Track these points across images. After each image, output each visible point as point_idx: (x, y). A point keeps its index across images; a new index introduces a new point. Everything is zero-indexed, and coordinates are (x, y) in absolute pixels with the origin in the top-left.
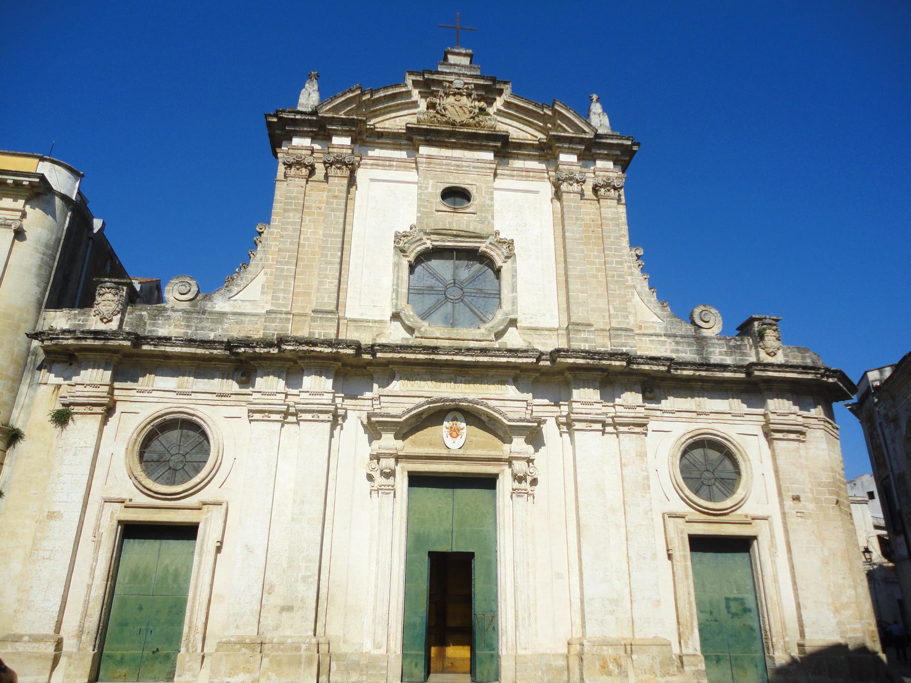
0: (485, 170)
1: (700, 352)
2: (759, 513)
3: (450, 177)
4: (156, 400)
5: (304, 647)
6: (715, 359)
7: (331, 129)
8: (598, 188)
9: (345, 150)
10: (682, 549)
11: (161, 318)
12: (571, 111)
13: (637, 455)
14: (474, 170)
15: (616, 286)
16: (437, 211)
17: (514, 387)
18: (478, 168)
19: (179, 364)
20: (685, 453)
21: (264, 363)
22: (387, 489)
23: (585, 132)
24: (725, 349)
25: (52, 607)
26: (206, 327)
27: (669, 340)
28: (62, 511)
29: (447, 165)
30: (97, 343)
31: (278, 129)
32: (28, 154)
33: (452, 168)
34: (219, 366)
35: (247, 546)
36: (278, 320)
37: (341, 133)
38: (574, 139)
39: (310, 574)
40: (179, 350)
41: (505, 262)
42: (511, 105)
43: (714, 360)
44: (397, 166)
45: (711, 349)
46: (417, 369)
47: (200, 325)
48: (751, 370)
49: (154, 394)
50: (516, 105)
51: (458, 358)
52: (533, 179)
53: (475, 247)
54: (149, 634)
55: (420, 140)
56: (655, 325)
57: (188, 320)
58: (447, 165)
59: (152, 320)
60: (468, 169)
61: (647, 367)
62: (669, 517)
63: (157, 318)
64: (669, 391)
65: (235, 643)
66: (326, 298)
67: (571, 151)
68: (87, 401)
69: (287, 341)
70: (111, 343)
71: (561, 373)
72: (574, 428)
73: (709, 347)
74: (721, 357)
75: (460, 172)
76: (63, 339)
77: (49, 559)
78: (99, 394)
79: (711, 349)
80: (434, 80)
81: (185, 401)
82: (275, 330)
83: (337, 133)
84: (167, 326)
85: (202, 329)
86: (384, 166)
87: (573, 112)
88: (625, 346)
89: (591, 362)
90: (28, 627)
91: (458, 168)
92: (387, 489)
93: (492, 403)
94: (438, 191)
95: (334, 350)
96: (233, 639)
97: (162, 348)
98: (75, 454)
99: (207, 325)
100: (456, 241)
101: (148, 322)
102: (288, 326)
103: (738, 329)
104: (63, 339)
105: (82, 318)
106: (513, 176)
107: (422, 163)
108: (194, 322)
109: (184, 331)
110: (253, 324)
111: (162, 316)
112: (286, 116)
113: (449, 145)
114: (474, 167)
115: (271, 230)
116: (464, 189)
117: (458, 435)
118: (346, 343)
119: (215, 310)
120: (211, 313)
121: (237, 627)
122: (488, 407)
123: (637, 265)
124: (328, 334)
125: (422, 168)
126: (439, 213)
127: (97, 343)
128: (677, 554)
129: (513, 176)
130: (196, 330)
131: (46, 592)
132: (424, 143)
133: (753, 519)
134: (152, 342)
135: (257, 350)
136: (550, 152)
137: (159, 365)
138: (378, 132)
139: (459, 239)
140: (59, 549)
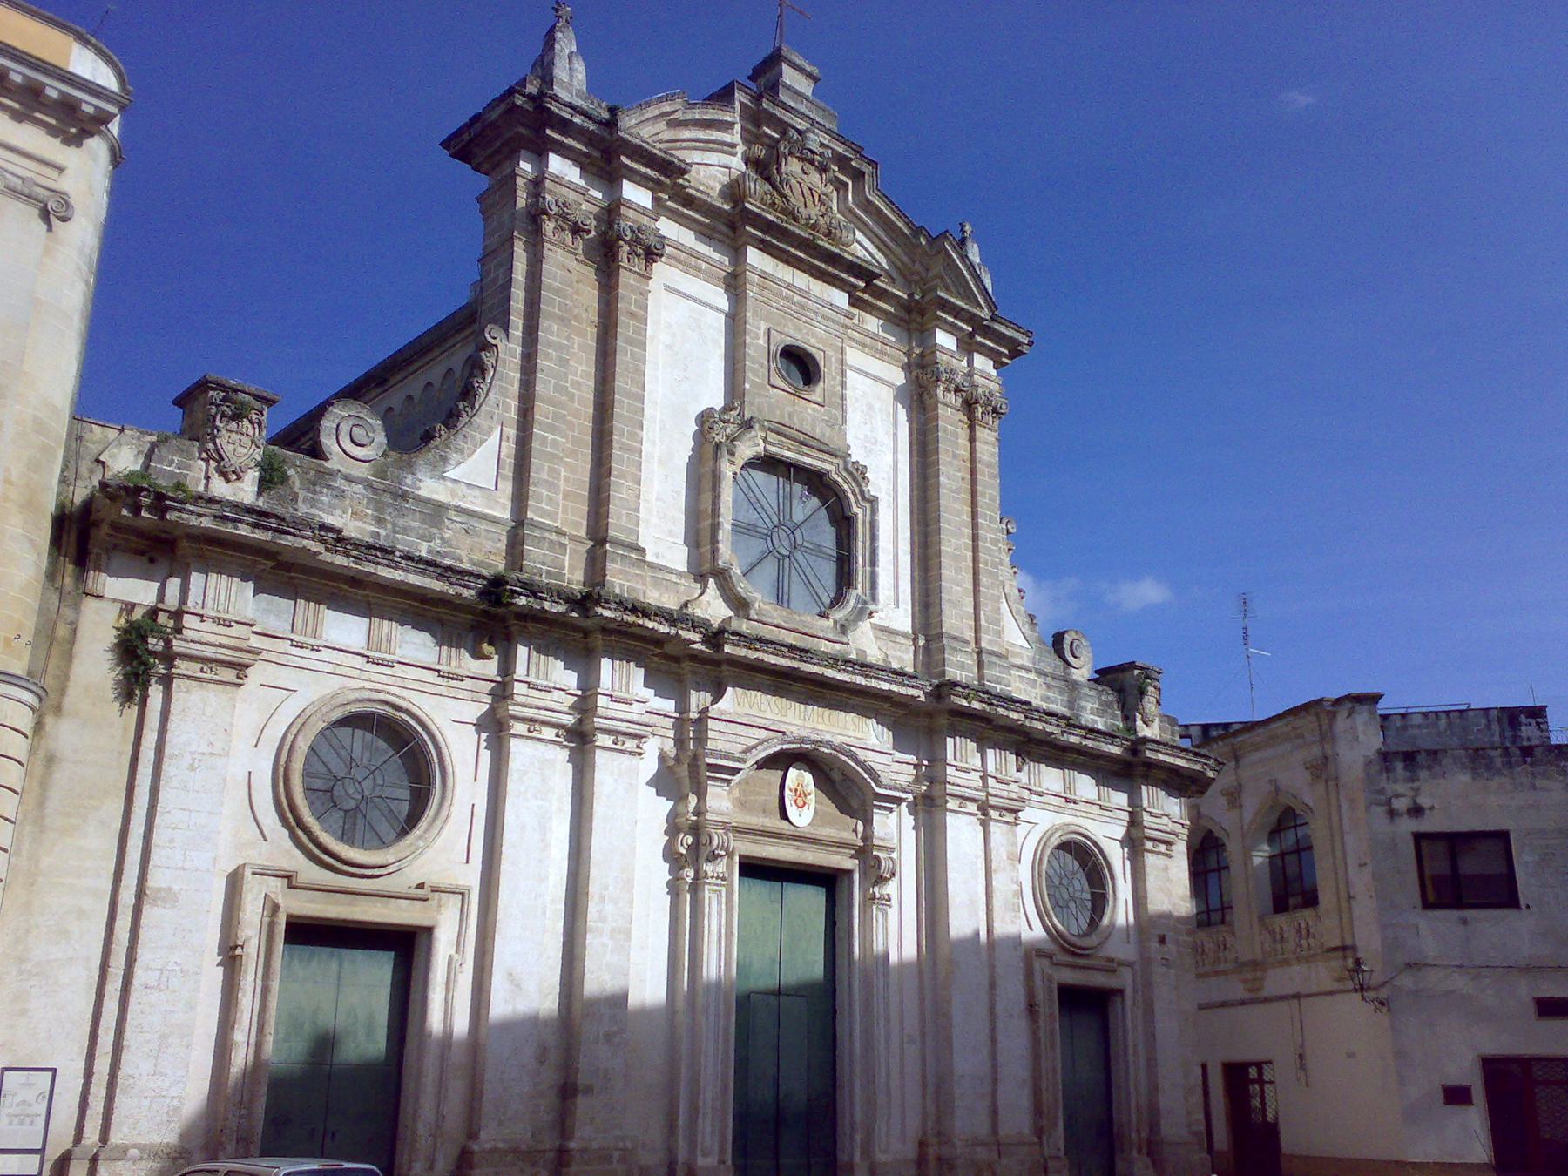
0: (836, 327)
1: (1071, 704)
2: (445, 881)
3: (790, 325)
4: (329, 668)
5: (616, 1155)
8: (545, 217)
10: (1049, 1007)
13: (1008, 858)
18: (829, 319)
21: (532, 627)
22: (717, 885)
25: (170, 1087)
26: (413, 529)
27: (1040, 680)
28: (176, 887)
30: (259, 535)
31: (523, 125)
33: (794, 308)
34: (445, 617)
35: (511, 974)
36: (546, 544)
37: (638, 178)
39: (615, 1028)
40: (402, 578)
44: (705, 272)
45: (1083, 703)
46: (759, 677)
47: (401, 522)
48: (1140, 747)
49: (325, 654)
52: (889, 360)
56: (1023, 652)
57: (379, 507)
59: (308, 490)
62: (254, 873)
63: (318, 489)
64: (547, 647)
66: (624, 518)
67: (952, 329)
68: (213, 656)
69: (607, 601)
70: (288, 541)
71: (716, 663)
72: (512, 732)
73: (1080, 699)
74: (1092, 717)
75: (804, 319)
76: (191, 512)
77: (158, 988)
79: (1083, 703)
80: (773, 115)
81: (384, 679)
82: (544, 564)
84: (339, 512)
85: (405, 530)
88: (1000, 683)
90: (125, 1130)
91: (801, 311)
92: (717, 885)
93: (862, 755)
95: (673, 631)
96: (501, 1145)
97: (370, 568)
98: (192, 768)
101: (302, 494)
102: (564, 560)
104: (191, 512)
105: (176, 459)
107: (753, 284)
109: (373, 528)
110: (492, 539)
111: (329, 487)
112: (557, 111)
113: (791, 260)
115: (510, 345)
116: (810, 355)
117: (805, 804)
118: (693, 622)
119: (420, 493)
121: (501, 1124)
122: (857, 761)
124: (634, 589)
126: (775, 390)
127: (259, 535)
128: (1043, 1010)
130: (395, 532)
131: (156, 1058)
133: (432, 891)
134: (354, 553)
135: (547, 605)
136: (919, 319)
137: (333, 594)
138: (688, 194)
139: (805, 449)
140: (177, 968)
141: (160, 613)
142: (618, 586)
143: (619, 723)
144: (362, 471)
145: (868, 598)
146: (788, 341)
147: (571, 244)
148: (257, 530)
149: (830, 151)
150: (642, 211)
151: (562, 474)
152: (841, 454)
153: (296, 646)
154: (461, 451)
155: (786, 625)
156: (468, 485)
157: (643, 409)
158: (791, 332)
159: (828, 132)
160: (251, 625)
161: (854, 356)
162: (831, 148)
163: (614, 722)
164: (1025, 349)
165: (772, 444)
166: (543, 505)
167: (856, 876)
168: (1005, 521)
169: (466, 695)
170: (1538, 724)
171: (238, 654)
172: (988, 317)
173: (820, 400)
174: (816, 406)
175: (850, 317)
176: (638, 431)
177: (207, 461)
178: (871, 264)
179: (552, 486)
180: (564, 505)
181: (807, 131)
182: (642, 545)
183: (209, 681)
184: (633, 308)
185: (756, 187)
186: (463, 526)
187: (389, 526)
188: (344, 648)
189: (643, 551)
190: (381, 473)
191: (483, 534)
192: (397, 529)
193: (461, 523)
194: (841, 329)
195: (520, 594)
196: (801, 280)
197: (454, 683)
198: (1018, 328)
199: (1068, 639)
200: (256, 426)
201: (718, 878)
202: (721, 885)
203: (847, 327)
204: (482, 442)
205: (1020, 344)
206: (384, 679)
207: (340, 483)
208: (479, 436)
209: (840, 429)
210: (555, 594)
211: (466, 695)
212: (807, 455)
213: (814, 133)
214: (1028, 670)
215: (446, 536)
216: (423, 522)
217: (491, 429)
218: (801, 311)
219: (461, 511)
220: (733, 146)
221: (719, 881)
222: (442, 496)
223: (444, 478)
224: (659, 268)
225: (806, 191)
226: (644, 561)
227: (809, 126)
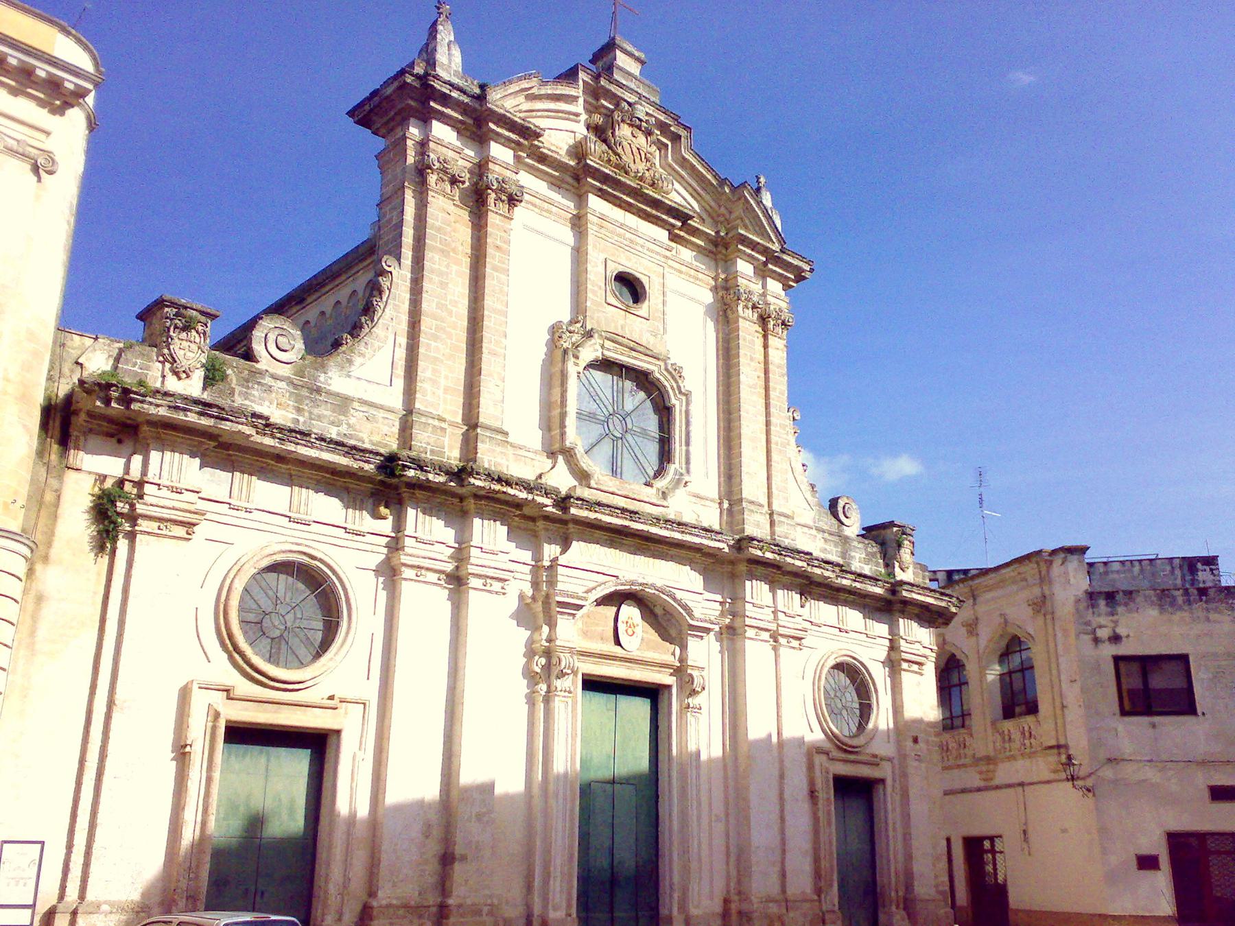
3: (622, 255)
4: (369, 547)
5: (486, 909)
6: (856, 566)
7: (493, 131)
10: (826, 793)
11: (256, 386)
14: (647, 252)
17: (702, 577)
18: (652, 251)
19: (293, 473)
20: (275, 568)
24: (863, 556)
27: (820, 535)
29: (619, 235)
30: (205, 422)
31: (412, 98)
32: (44, 14)
36: (430, 429)
37: (503, 141)
38: (758, 246)
39: (485, 810)
42: (686, 164)
43: (856, 568)
46: (598, 533)
47: (316, 411)
48: (898, 588)
50: (693, 166)
51: (654, 530)
53: (648, 369)
54: (258, 898)
55: (593, 186)
58: (619, 235)
59: (242, 386)
60: (641, 249)
61: (818, 571)
63: (250, 385)
65: (398, 907)
69: (478, 474)
71: (564, 522)
73: (851, 550)
78: (178, 505)
80: (608, 91)
82: (428, 444)
83: (498, 137)
85: (319, 418)
86: (542, 209)
89: (778, 557)
93: (679, 595)
96: (394, 902)
97: (291, 447)
99: (326, 413)
100: (629, 357)
101: (238, 389)
103: (864, 529)
106: (680, 272)
108: (307, 405)
111: (259, 383)
112: (438, 87)
113: (623, 205)
114: (648, 249)
116: (638, 280)
120: (329, 393)
121: (394, 885)
122: (675, 599)
123: (793, 432)
124: (499, 464)
125: (592, 232)
127: (205, 422)
128: (821, 795)
129: (680, 272)
130: (311, 419)
132: (595, 192)
135: (431, 477)
137: (262, 468)
139: (634, 354)
144: (285, 371)
145: (684, 471)
146: (621, 269)
147: (449, 192)
155: (619, 493)
159: (652, 104)
164: (807, 275)
165: (608, 350)
167: (674, 690)
170: (1211, 570)
172: (778, 250)
177: (163, 363)
186: (365, 414)
187: (307, 414)
190: (300, 373)
191: (381, 420)
195: (410, 468)
198: (802, 259)
199: (841, 503)
201: (565, 691)
202: (568, 697)
203: (667, 257)
205: (804, 271)
207: (268, 380)
210: (437, 467)
213: (641, 105)
215: (351, 422)
216: (334, 411)
220: (577, 115)
221: (567, 694)
225: (635, 150)
227: (637, 99)
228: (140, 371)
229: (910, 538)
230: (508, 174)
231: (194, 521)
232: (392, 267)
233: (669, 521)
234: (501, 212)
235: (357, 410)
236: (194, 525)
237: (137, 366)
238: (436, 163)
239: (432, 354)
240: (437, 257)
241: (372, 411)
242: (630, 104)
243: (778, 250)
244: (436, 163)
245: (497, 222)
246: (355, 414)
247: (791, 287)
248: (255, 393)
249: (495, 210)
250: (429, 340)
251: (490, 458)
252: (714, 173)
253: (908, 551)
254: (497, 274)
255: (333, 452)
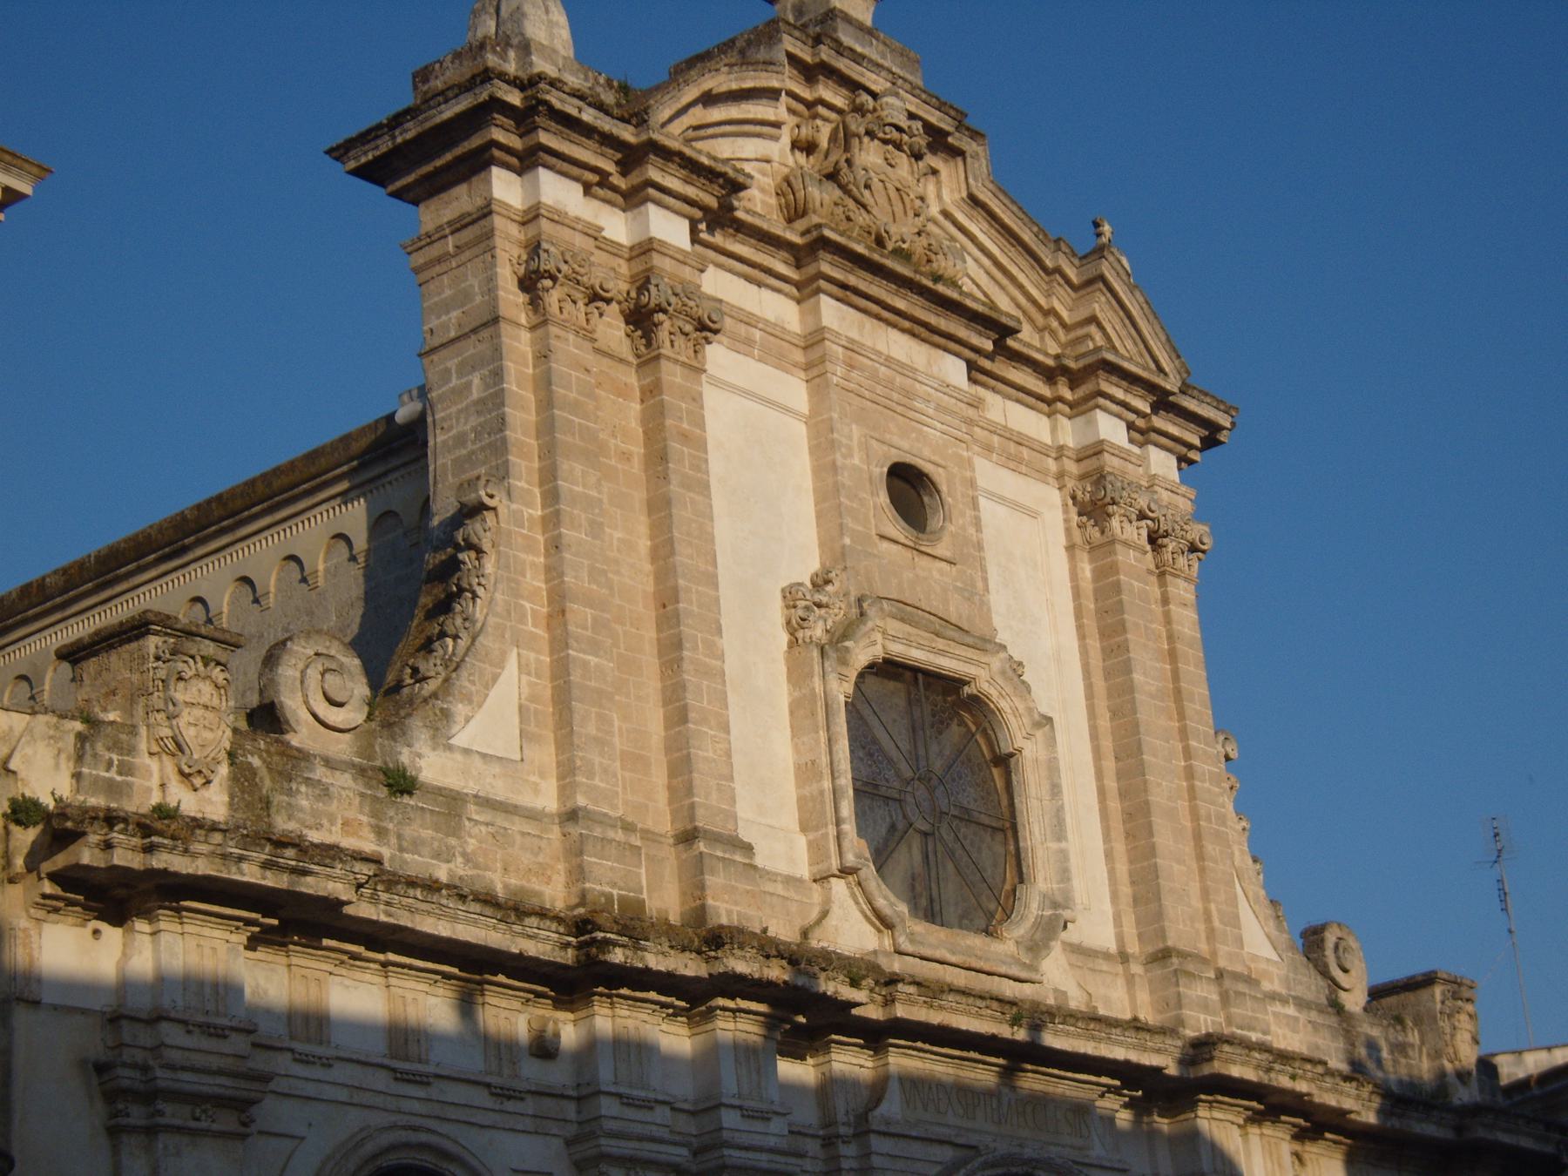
3: (891, 425)
4: (342, 1095)
9: (688, 269)
11: (303, 789)
12: (1138, 294)
15: (1217, 848)
16: (882, 537)
23: (1160, 370)
27: (1303, 1017)
41: (1029, 736)
49: (341, 1073)
66: (714, 795)
81: (417, 1107)
85: (416, 845)
87: (1141, 299)
94: (877, 470)
102: (639, 875)
111: (308, 781)
115: (514, 506)
130: (401, 849)
139: (940, 644)
141: (124, 1023)
142: (723, 913)
143: (757, 1155)
144: (341, 747)
147: (584, 324)
148: (268, 873)
149: (919, 124)
150: (681, 258)
151: (616, 723)
152: (985, 643)
153: (302, 1061)
154: (468, 699)
155: (953, 959)
156: (484, 756)
157: (717, 600)
158: (896, 440)
159: (913, 90)
160: (250, 1032)
161: (989, 474)
162: (920, 119)
163: (751, 1155)
164: (1223, 436)
165: (895, 638)
166: (597, 782)
168: (1221, 738)
169: (528, 1124)
171: (243, 1084)
172: (1176, 390)
173: (947, 554)
174: (944, 564)
175: (976, 404)
176: (716, 639)
178: (975, 299)
179: (602, 743)
180: (624, 778)
181: (886, 93)
182: (745, 835)
183: (205, 1133)
184: (685, 426)
185: (822, 196)
186: (490, 829)
187: (394, 840)
188: (363, 1058)
189: (748, 849)
190: (366, 751)
191: (518, 838)
192: (405, 844)
193: (487, 824)
194: (964, 428)
195: (615, 944)
196: (899, 345)
197: (510, 1106)
198: (1219, 404)
199: (1330, 938)
200: (222, 691)
204: (495, 678)
205: (1220, 428)
206: (407, 1105)
207: (320, 773)
208: (488, 668)
209: (982, 603)
211: (528, 1124)
212: (943, 653)
213: (897, 95)
214: (1284, 1001)
215: (469, 849)
216: (437, 830)
217: (503, 656)
218: (905, 401)
219: (487, 803)
220: (777, 125)
222: (453, 781)
223: (450, 748)
224: (717, 354)
225: (893, 194)
226: (755, 867)
227: (889, 85)
228: (119, 778)
229: (1469, 1007)
230: (687, 273)
231: (253, 1095)
232: (497, 498)
233: (1071, 1016)
234: (683, 358)
235: (477, 822)
236: (253, 1102)
237: (114, 769)
238: (673, 300)
239: (593, 684)
240: (578, 468)
241: (501, 820)
242: (874, 95)
243: (1176, 390)
244: (673, 300)
245: (678, 380)
246: (475, 830)
247: (1191, 462)
248: (304, 803)
249: (673, 355)
250: (585, 652)
251: (728, 906)
252: (1035, 229)
253: (1467, 1036)
254: (692, 495)
255: (475, 922)
